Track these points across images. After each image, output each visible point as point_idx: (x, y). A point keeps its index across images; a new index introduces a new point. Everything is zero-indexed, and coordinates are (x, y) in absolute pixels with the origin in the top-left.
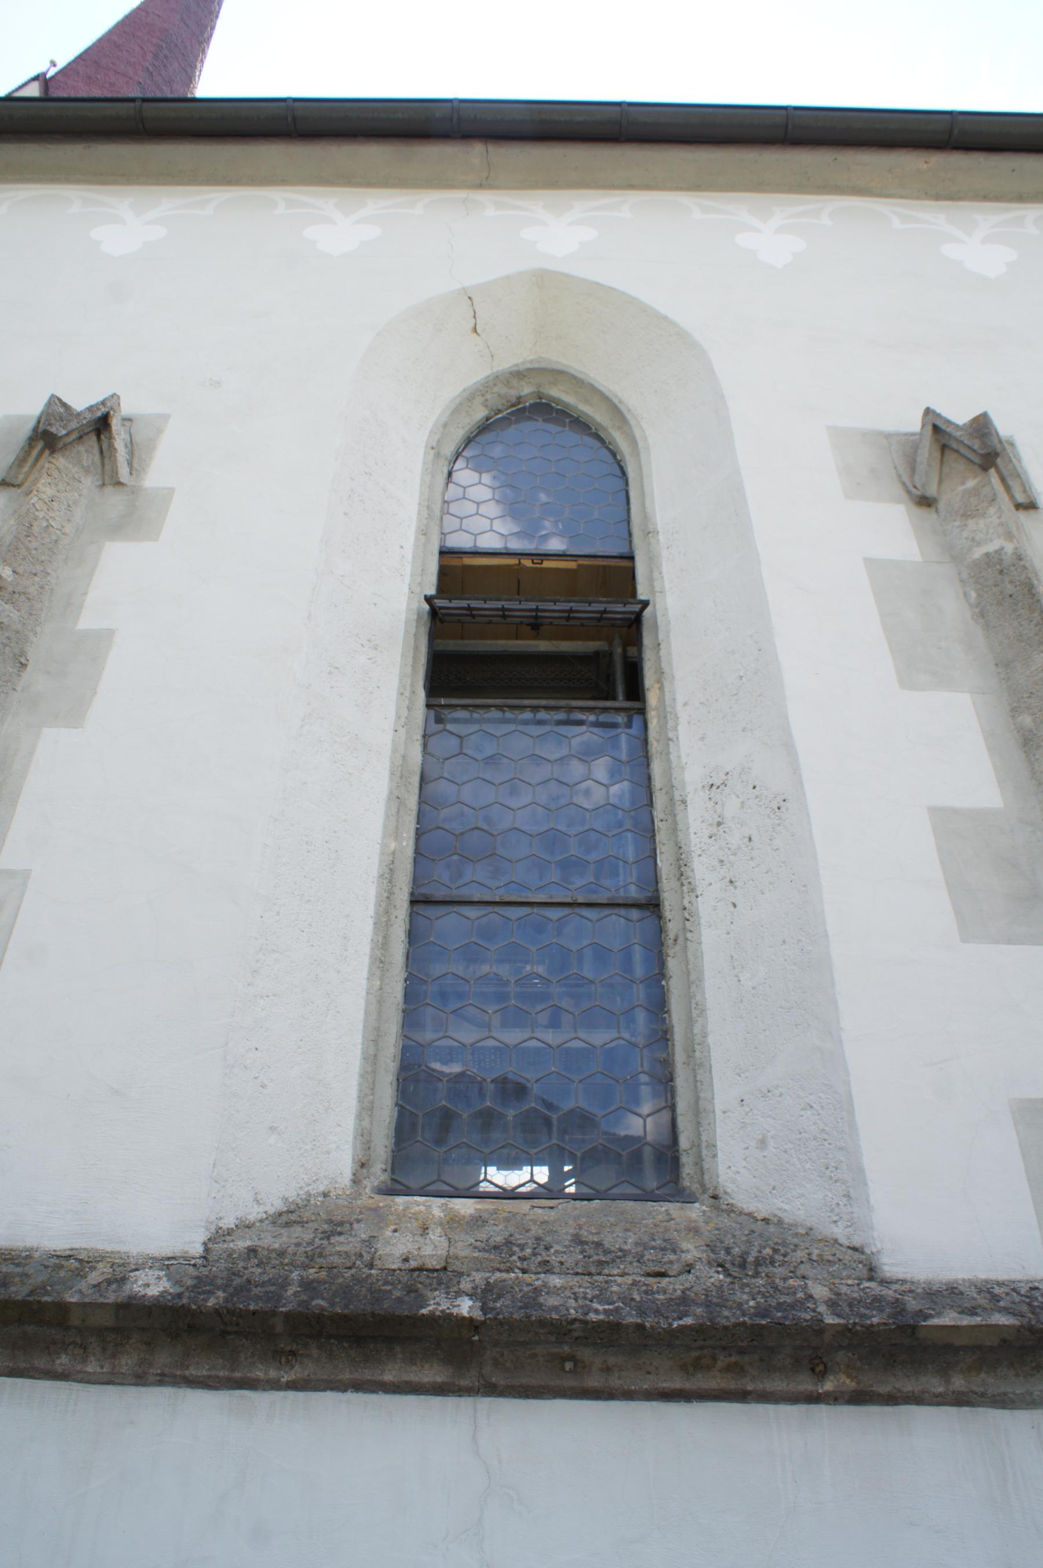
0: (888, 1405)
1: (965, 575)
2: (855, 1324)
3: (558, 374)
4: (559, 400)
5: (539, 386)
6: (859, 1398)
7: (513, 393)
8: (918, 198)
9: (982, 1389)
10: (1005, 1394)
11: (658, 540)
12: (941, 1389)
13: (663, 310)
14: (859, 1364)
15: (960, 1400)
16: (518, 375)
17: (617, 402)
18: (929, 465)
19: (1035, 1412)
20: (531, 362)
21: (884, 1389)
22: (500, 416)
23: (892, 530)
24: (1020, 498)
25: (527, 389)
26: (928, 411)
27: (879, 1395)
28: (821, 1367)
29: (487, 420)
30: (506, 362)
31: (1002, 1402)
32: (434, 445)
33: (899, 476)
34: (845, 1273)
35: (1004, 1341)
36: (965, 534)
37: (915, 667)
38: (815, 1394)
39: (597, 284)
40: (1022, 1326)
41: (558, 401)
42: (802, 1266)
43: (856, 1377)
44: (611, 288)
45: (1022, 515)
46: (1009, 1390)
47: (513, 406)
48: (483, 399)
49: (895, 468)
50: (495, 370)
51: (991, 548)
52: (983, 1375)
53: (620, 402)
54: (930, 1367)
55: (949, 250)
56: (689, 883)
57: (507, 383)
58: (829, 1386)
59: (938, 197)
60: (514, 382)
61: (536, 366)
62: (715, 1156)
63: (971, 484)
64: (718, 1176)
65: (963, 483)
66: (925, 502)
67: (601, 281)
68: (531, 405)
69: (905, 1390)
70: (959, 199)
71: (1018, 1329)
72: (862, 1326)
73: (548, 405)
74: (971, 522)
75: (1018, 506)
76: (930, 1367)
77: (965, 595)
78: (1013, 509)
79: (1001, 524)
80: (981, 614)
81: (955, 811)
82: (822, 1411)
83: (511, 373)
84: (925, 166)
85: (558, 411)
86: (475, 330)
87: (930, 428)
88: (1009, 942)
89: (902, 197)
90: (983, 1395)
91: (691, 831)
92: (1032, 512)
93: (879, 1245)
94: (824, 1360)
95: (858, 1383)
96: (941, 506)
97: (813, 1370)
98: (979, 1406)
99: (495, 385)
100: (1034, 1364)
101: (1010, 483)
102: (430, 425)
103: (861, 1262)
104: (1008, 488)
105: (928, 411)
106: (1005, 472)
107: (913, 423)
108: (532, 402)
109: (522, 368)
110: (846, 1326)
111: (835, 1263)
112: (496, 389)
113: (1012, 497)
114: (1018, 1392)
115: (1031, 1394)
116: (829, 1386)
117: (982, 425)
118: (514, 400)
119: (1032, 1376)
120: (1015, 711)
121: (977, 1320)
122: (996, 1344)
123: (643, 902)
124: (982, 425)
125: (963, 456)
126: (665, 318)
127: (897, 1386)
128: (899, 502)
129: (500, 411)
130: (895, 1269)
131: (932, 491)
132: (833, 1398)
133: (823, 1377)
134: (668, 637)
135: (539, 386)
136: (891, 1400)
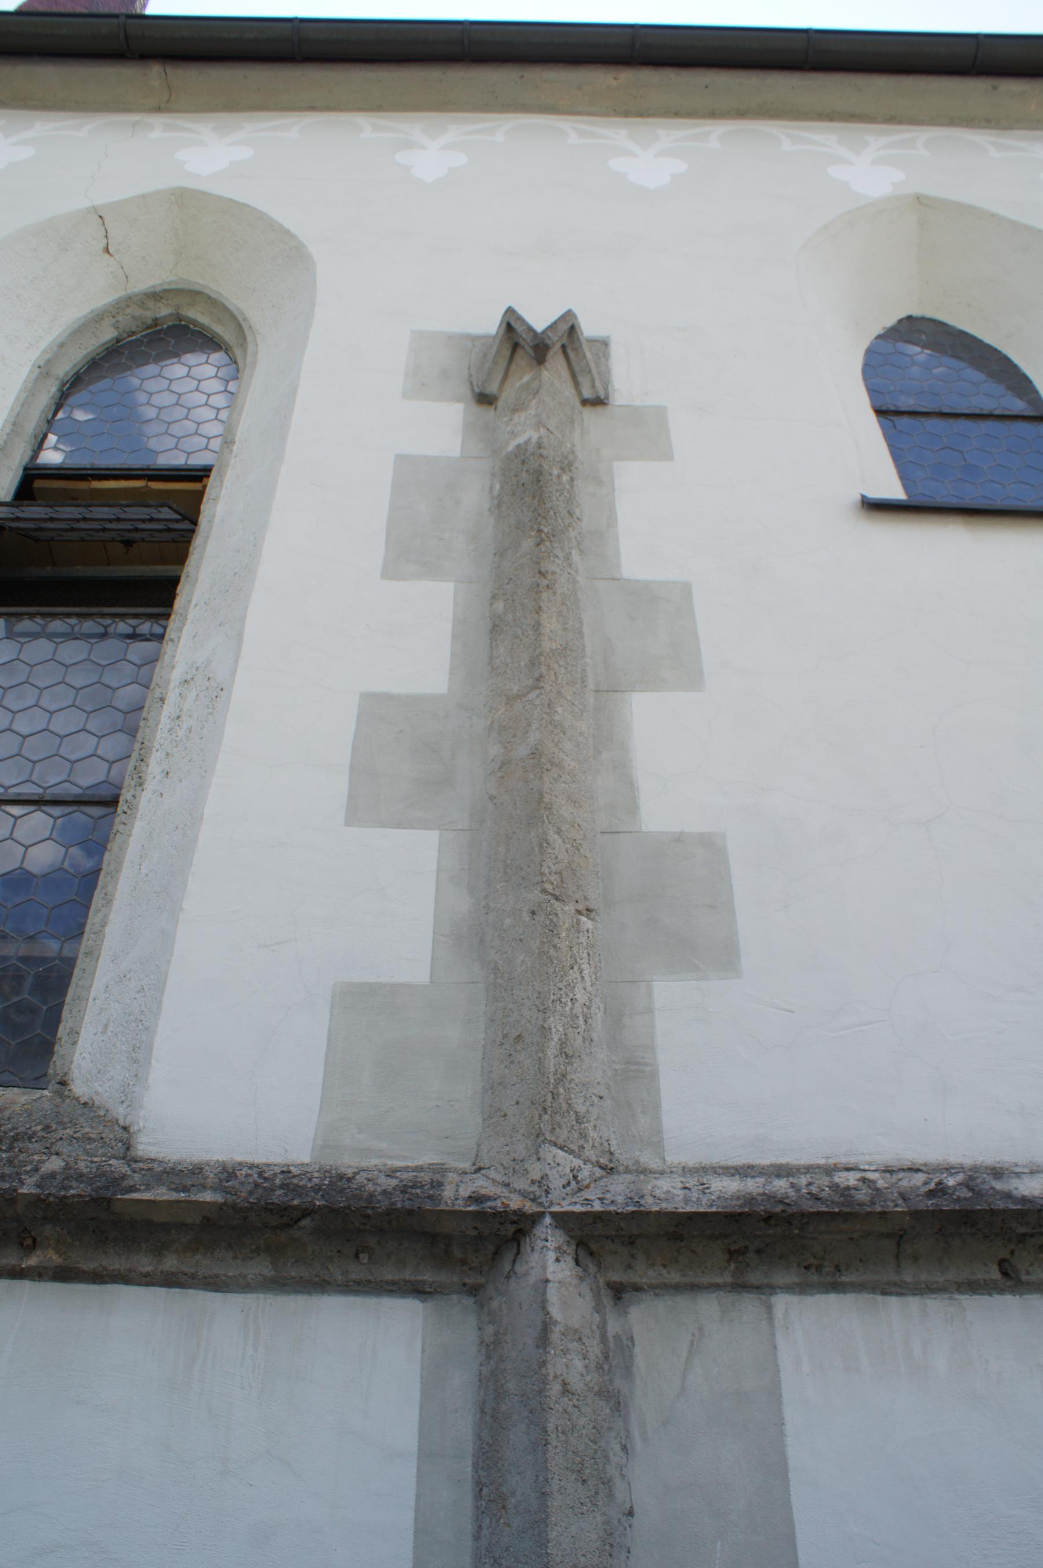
0: (94, 1283)
2: (50, 1194)
3: (195, 295)
4: (196, 321)
5: (178, 307)
6: (64, 1275)
7: (149, 315)
8: (606, 115)
9: (193, 1271)
10: (217, 1276)
11: (231, 451)
12: (149, 1269)
13: (287, 224)
14: (69, 1240)
15: (170, 1281)
16: (156, 296)
17: (241, 320)
18: (495, 363)
19: (249, 1296)
20: (170, 283)
21: (88, 1266)
22: (134, 338)
23: (442, 428)
24: (587, 393)
25: (164, 311)
26: (510, 311)
27: (84, 1272)
28: (29, 1242)
29: (118, 342)
30: (141, 284)
31: (214, 1284)
32: (42, 364)
33: (470, 375)
34: (101, 1151)
35: (207, 1219)
37: (407, 554)
38: (18, 1269)
39: (232, 200)
40: (225, 1203)
41: (195, 323)
42: (60, 1143)
43: (65, 1253)
44: (244, 204)
45: (588, 412)
46: (222, 1272)
47: (148, 328)
48: (114, 321)
49: (469, 368)
50: (130, 291)
51: (521, 440)
52: (199, 1257)
53: (245, 319)
54: (144, 1246)
56: (140, 777)
57: (142, 305)
58: (33, 1261)
59: (627, 114)
60: (151, 304)
61: (173, 287)
62: (75, 1043)
63: (526, 378)
64: (72, 1063)
65: (521, 378)
66: (485, 399)
67: (235, 198)
68: (170, 328)
69: (111, 1268)
70: (649, 116)
71: (220, 1207)
72: (56, 1197)
73: (186, 327)
74: (516, 417)
75: (585, 402)
76: (144, 1246)
77: (491, 488)
78: (578, 404)
79: (536, 415)
80: (498, 506)
81: (389, 697)
82: (25, 1287)
83: (145, 294)
84: (615, 83)
85: (194, 332)
86: (107, 250)
87: (504, 326)
88: (399, 825)
89: (589, 114)
90: (193, 1276)
91: (160, 727)
92: (599, 408)
93: (141, 1125)
94: (33, 1233)
95: (65, 1259)
96: (500, 403)
97: (22, 1244)
98: (190, 1288)
99: (128, 306)
100: (254, 1247)
101: (580, 379)
102: (44, 345)
103: (121, 1141)
104: (577, 384)
105: (510, 311)
106: (577, 368)
107: (490, 325)
108: (170, 324)
109: (158, 290)
110: (38, 1196)
111: (95, 1141)
112: (129, 311)
114: (230, 1274)
115: (245, 1276)
116: (33, 1261)
117: (568, 328)
118: (149, 322)
119: (251, 1259)
120: (494, 597)
121: (182, 1195)
122: (198, 1221)
123: (109, 799)
124: (568, 328)
126: (287, 232)
127: (104, 1264)
128: (459, 400)
129: (134, 333)
130: (150, 1148)
131: (493, 388)
132: (37, 1274)
133: (30, 1252)
134: (206, 542)
135: (178, 307)
136: (98, 1278)
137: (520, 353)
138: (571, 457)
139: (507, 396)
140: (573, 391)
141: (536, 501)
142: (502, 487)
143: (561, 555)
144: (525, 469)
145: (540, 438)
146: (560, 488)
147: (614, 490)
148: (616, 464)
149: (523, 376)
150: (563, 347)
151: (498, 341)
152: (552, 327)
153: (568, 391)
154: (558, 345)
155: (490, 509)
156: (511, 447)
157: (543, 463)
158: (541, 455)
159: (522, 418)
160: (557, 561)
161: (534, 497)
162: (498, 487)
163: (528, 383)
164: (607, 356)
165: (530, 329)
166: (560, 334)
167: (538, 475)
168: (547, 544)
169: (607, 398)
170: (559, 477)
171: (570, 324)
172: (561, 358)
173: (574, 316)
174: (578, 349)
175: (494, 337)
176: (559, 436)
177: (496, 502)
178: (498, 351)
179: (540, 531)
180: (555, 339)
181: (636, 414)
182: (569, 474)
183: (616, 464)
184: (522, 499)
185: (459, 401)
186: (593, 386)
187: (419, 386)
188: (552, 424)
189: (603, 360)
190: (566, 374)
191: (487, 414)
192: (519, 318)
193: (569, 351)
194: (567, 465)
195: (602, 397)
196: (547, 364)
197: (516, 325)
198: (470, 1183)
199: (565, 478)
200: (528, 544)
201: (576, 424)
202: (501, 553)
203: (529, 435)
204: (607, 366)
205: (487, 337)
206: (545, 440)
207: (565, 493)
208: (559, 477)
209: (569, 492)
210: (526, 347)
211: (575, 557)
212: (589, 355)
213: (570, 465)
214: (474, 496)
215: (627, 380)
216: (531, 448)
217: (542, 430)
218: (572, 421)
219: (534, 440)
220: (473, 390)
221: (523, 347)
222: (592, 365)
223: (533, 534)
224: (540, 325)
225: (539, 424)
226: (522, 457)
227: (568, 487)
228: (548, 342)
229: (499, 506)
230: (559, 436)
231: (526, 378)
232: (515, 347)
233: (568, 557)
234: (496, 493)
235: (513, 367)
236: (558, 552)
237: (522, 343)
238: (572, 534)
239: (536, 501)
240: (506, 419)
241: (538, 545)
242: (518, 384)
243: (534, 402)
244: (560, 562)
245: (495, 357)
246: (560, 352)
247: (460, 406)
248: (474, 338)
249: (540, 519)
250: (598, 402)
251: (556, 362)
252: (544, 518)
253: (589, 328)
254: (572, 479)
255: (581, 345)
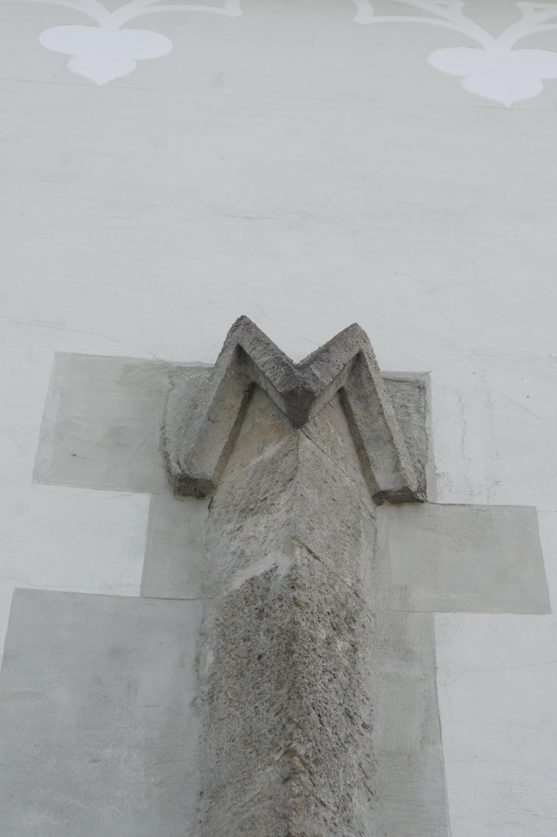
1: (210, 623)
23: (103, 542)
24: (385, 481)
26: (243, 324)
33: (165, 441)
36: (235, 544)
45: (385, 515)
51: (258, 569)
55: (444, 60)
63: (270, 451)
65: (261, 451)
66: (191, 487)
74: (249, 523)
75: (380, 497)
87: (231, 351)
92: (407, 509)
96: (220, 496)
105: (243, 324)
106: (366, 434)
107: (206, 347)
113: (370, 479)
117: (350, 357)
124: (350, 357)
125: (275, 405)
131: (206, 467)
137: (259, 403)
138: (352, 604)
139: (234, 482)
140: (359, 476)
141: (284, 690)
142: (218, 660)
143: (330, 801)
144: (264, 627)
145: (294, 567)
146: (330, 665)
147: (435, 669)
148: (439, 618)
149: (265, 447)
150: (342, 393)
151: (218, 379)
152: (320, 356)
153: (349, 477)
154: (333, 390)
155: (193, 704)
156: (238, 582)
157: (298, 617)
158: (296, 602)
159: (261, 528)
160: (323, 813)
161: (280, 684)
162: (210, 658)
163: (273, 461)
164: (423, 411)
165: (281, 360)
166: (335, 371)
167: (290, 640)
168: (305, 778)
169: (423, 490)
170: (329, 642)
171: (356, 351)
172: (337, 414)
173: (365, 339)
174: (369, 398)
175: (213, 370)
176: (330, 562)
177: (206, 689)
178: (218, 399)
179: (290, 752)
180: (326, 381)
181: (478, 522)
182: (349, 637)
183: (439, 618)
184: (257, 686)
185: (141, 489)
186: (397, 468)
187: (66, 457)
188: (318, 540)
189: (416, 417)
190: (345, 443)
191: (196, 513)
192: (261, 339)
193: (352, 400)
194: (344, 621)
195: (414, 488)
196: (310, 426)
197: (254, 352)
198: (220, 695)
199: (341, 645)
200: (266, 776)
201: (363, 540)
202: (213, 794)
203: (276, 560)
204: (423, 429)
205: (199, 369)
206: (304, 572)
207: (340, 674)
208: (329, 642)
209: (347, 673)
210: (271, 393)
211: (359, 805)
212: (389, 409)
213: (351, 619)
214: (165, 677)
215: (460, 458)
216: (276, 587)
217: (298, 552)
218: (356, 535)
219: (283, 572)
220: (169, 470)
221: (266, 392)
222: (395, 428)
223: (277, 757)
224: (297, 350)
225: (294, 541)
226: (259, 604)
227: (346, 663)
228: (314, 387)
229: (211, 697)
230: (330, 562)
231: (270, 451)
232: (251, 391)
233: (343, 806)
234: (206, 671)
235: (245, 429)
236: (324, 794)
237: (264, 385)
238: (353, 757)
239: (284, 690)
240: (230, 527)
241: (286, 780)
242: (254, 462)
243: (285, 497)
244: (329, 815)
245: (212, 409)
246: (335, 402)
247: (143, 500)
248: (174, 371)
249: (290, 728)
250: (406, 498)
251: (327, 422)
252: (298, 726)
253: (389, 357)
254: (354, 648)
255: (375, 392)
